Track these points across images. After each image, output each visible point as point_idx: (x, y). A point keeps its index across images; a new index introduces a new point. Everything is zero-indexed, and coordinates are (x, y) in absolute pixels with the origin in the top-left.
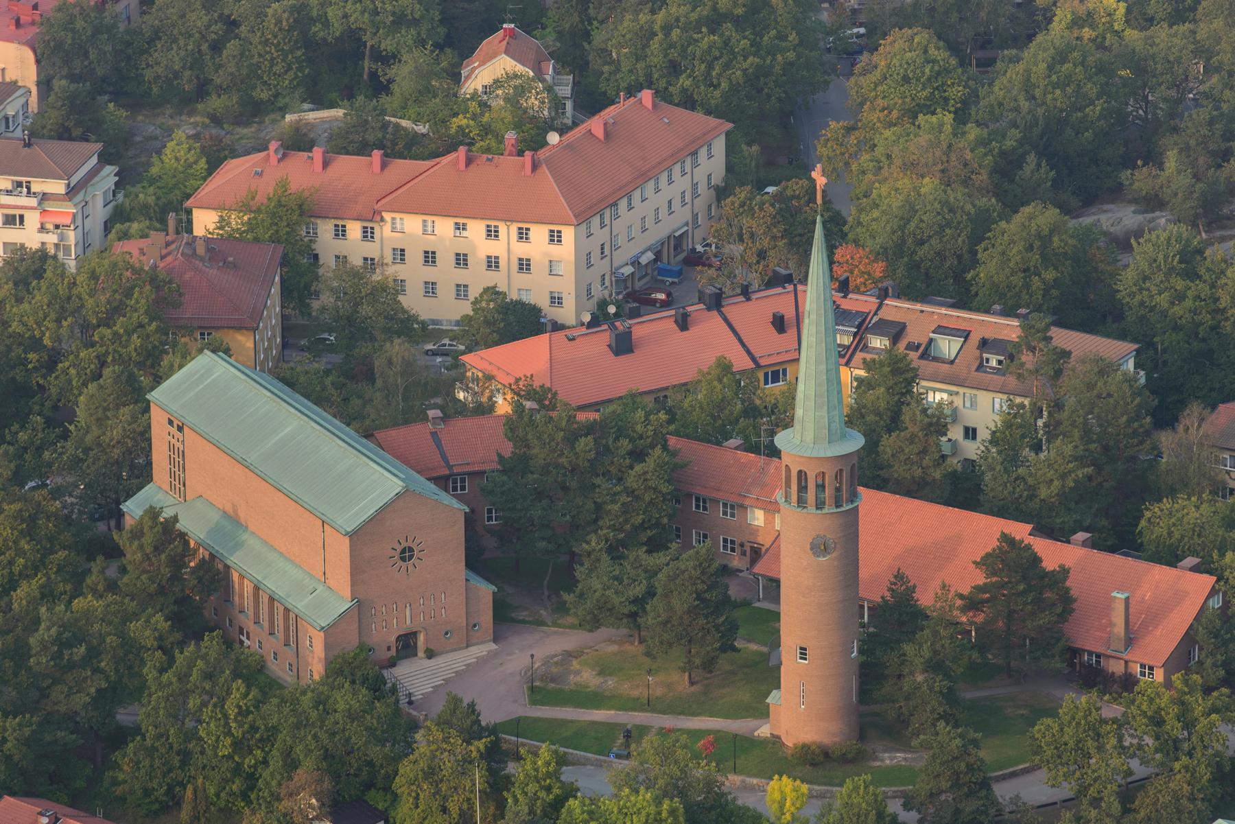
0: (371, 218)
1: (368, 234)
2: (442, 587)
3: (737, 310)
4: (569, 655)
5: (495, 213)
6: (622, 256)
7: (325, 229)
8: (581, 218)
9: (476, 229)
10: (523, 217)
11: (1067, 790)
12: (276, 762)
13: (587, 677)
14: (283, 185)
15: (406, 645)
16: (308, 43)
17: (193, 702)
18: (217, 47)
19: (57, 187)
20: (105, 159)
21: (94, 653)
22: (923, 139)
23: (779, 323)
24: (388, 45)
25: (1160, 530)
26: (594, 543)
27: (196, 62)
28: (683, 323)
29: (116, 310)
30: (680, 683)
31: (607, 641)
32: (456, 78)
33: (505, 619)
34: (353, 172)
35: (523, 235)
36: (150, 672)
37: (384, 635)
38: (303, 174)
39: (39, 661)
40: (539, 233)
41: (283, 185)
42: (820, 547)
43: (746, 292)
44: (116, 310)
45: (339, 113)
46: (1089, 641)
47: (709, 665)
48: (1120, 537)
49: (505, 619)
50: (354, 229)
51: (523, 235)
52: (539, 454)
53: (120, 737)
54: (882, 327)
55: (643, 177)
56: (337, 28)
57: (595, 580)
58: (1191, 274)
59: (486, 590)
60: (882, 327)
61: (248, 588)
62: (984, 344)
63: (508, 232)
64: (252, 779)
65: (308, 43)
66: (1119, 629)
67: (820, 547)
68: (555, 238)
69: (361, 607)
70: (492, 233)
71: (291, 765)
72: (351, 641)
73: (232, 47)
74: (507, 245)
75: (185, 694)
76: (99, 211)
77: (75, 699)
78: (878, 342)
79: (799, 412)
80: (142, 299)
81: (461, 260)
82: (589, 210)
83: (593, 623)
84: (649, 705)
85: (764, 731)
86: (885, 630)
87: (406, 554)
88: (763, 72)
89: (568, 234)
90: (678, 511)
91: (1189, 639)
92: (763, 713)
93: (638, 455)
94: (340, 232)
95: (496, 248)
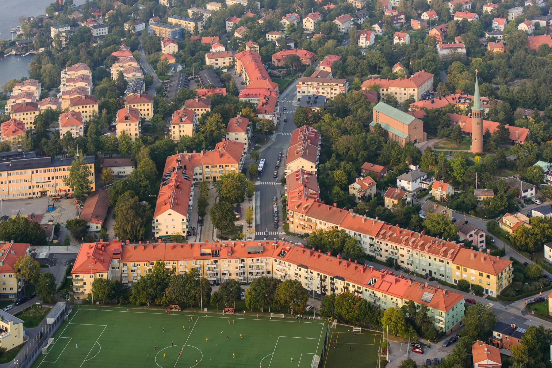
0: (387, 88)
1: (387, 90)
2: (420, 133)
3: (447, 97)
4: (438, 143)
5: (405, 87)
6: (422, 93)
7: (381, 90)
8: (418, 87)
9: (403, 89)
10: (409, 87)
11: (516, 158)
12: (403, 156)
13: (442, 145)
14: (375, 83)
15: (415, 141)
16: (370, 66)
17: (390, 148)
18: (357, 67)
19: (342, 85)
20: (347, 81)
21: (375, 142)
22: (464, 75)
23: (453, 99)
24: (382, 66)
25: (518, 124)
26: (440, 127)
27: (354, 69)
28: (440, 99)
29: (359, 100)
30: (456, 146)
31: (443, 141)
32: (392, 71)
33: (428, 138)
34: (384, 82)
35: (409, 90)
36: (383, 144)
37: (413, 140)
38: (378, 82)
39: (368, 143)
40: (412, 89)
41: (375, 83)
42: (478, 124)
43: (448, 95)
44: (359, 100)
45: (116, 170)
46: (512, 138)
47: (460, 142)
48: (512, 124)
49: (428, 138)
50: (385, 90)
51: (409, 90)
52: (430, 115)
53: (379, 155)
54: (468, 99)
55: (425, 82)
56: (374, 64)
57: (441, 132)
58: (508, 92)
59: (426, 133)
60: (468, 99)
61: (391, 134)
62: (483, 101)
63: (407, 89)
64: (399, 159)
65: (370, 66)
66: (517, 136)
67: (478, 124)
68: (414, 90)
69: (410, 136)
70: (405, 90)
71: (406, 157)
72: (408, 141)
73: (359, 67)
74: (407, 91)
75: (389, 147)
76: (347, 89)
77: (373, 148)
78: (468, 101)
79: (474, 104)
80: (363, 98)
81: (400, 94)
82: (419, 86)
83: (442, 137)
84: (452, 149)
85: (469, 151)
86: (486, 136)
87: (415, 128)
88: (436, 68)
89: (416, 89)
90: (449, 123)
91: (527, 138)
92: (470, 149)
93: (444, 115)
94: (383, 90)
95: (405, 92)
